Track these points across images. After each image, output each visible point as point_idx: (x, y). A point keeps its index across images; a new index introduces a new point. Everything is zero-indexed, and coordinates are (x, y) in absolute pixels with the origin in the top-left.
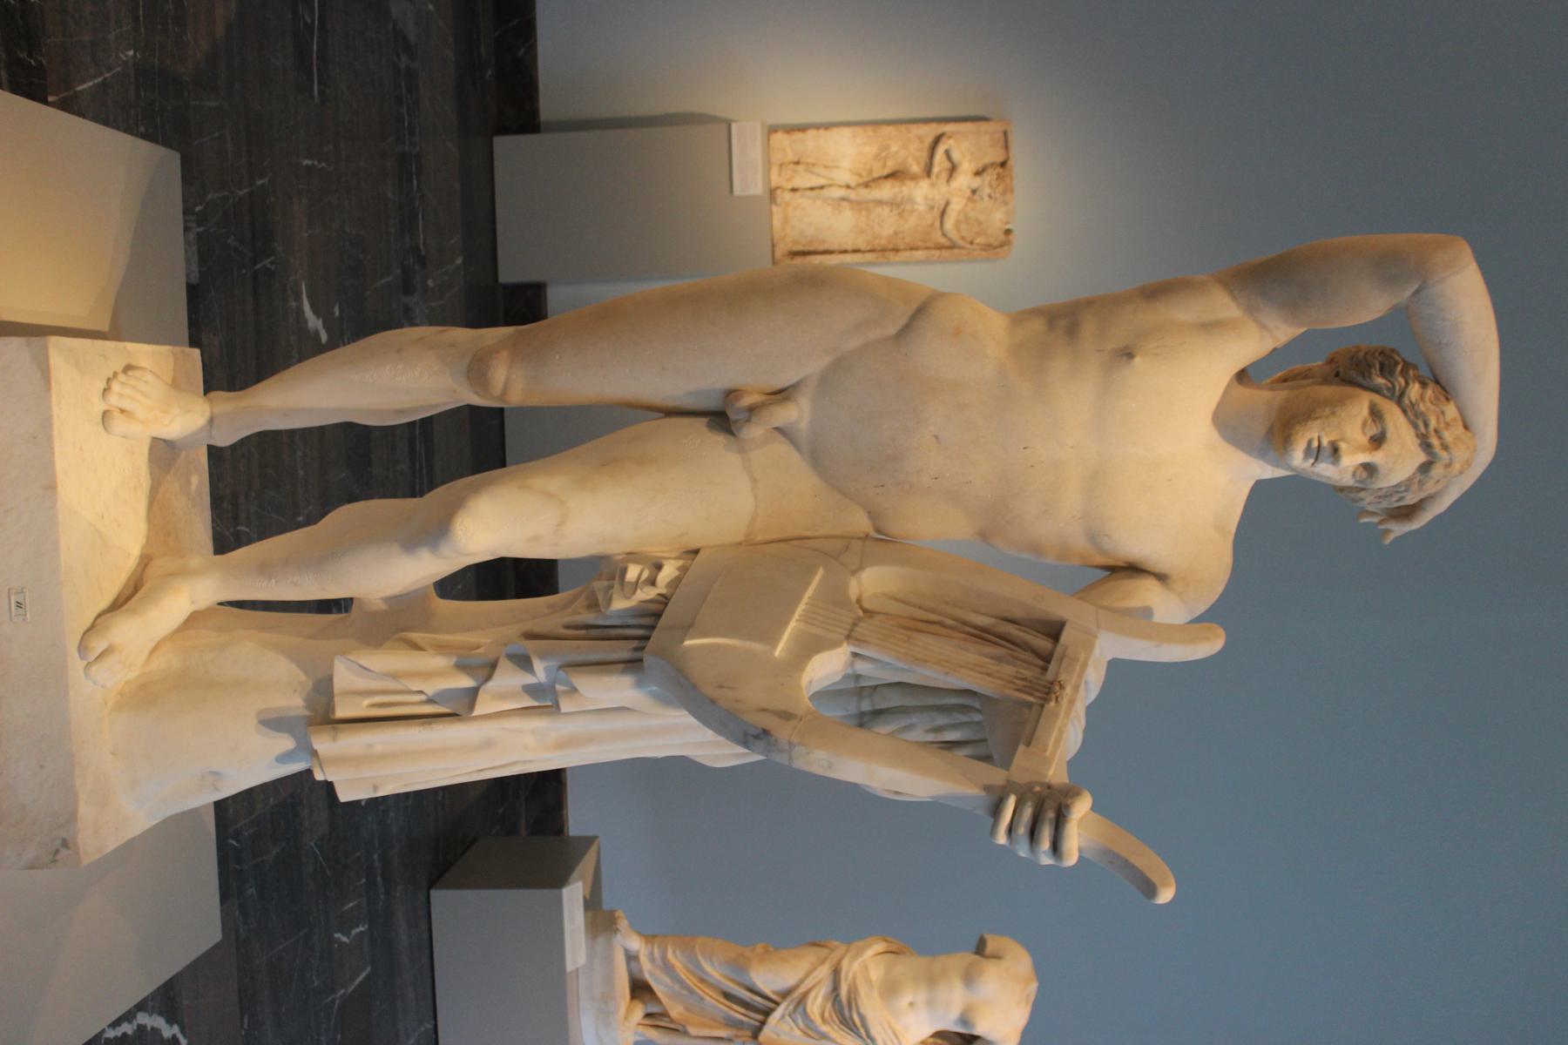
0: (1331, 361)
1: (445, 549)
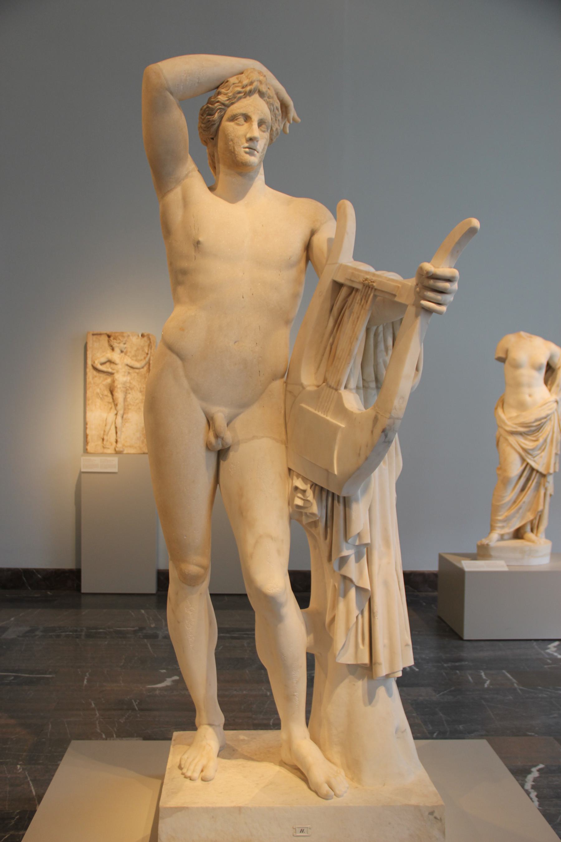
0: (206, 143)
1: (282, 599)
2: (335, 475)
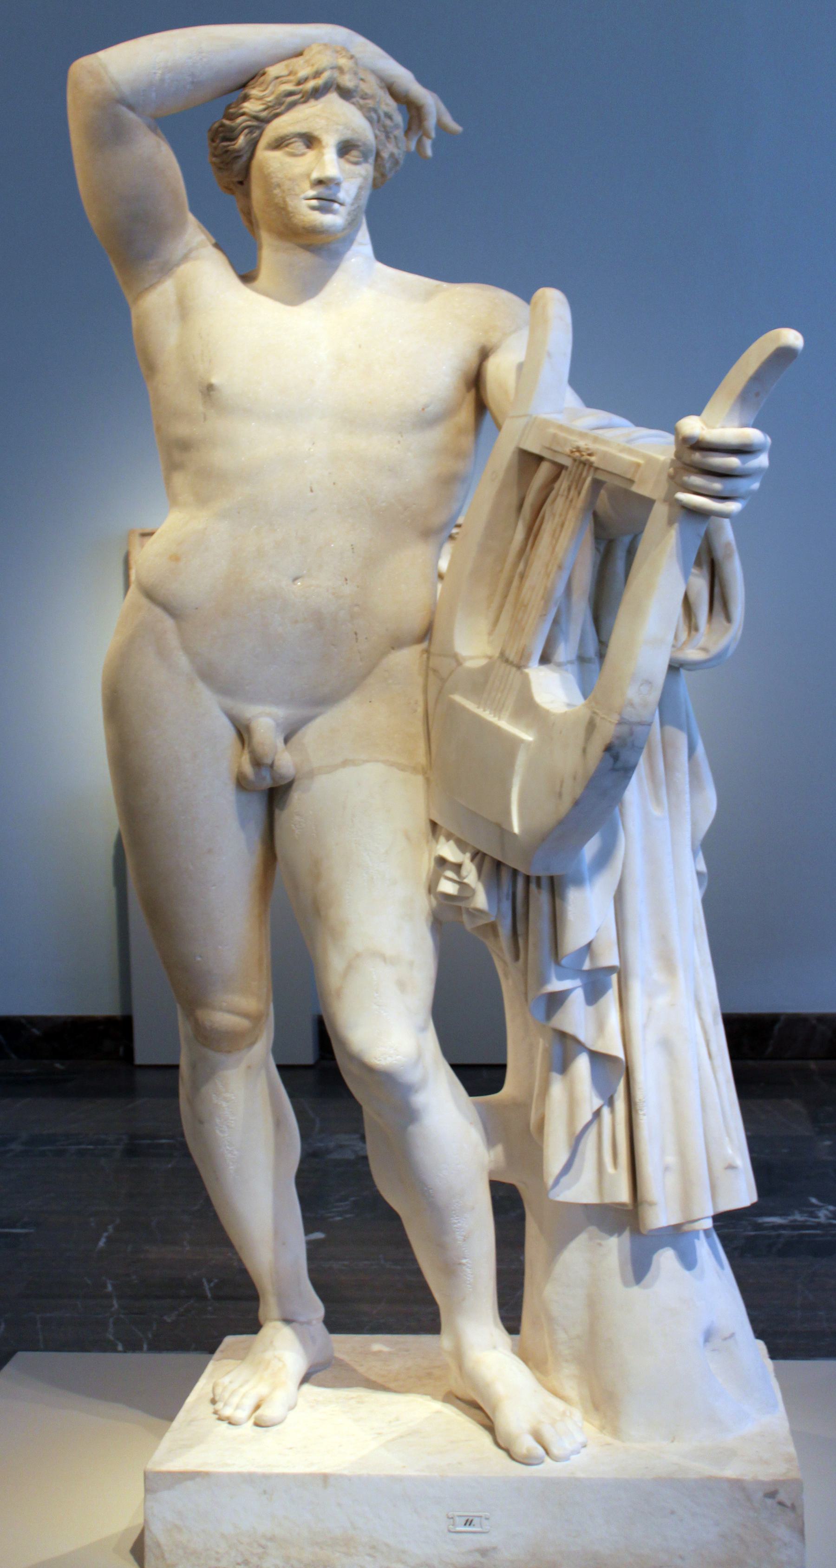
0: (229, 189)
1: (413, 1077)
2: (515, 834)
